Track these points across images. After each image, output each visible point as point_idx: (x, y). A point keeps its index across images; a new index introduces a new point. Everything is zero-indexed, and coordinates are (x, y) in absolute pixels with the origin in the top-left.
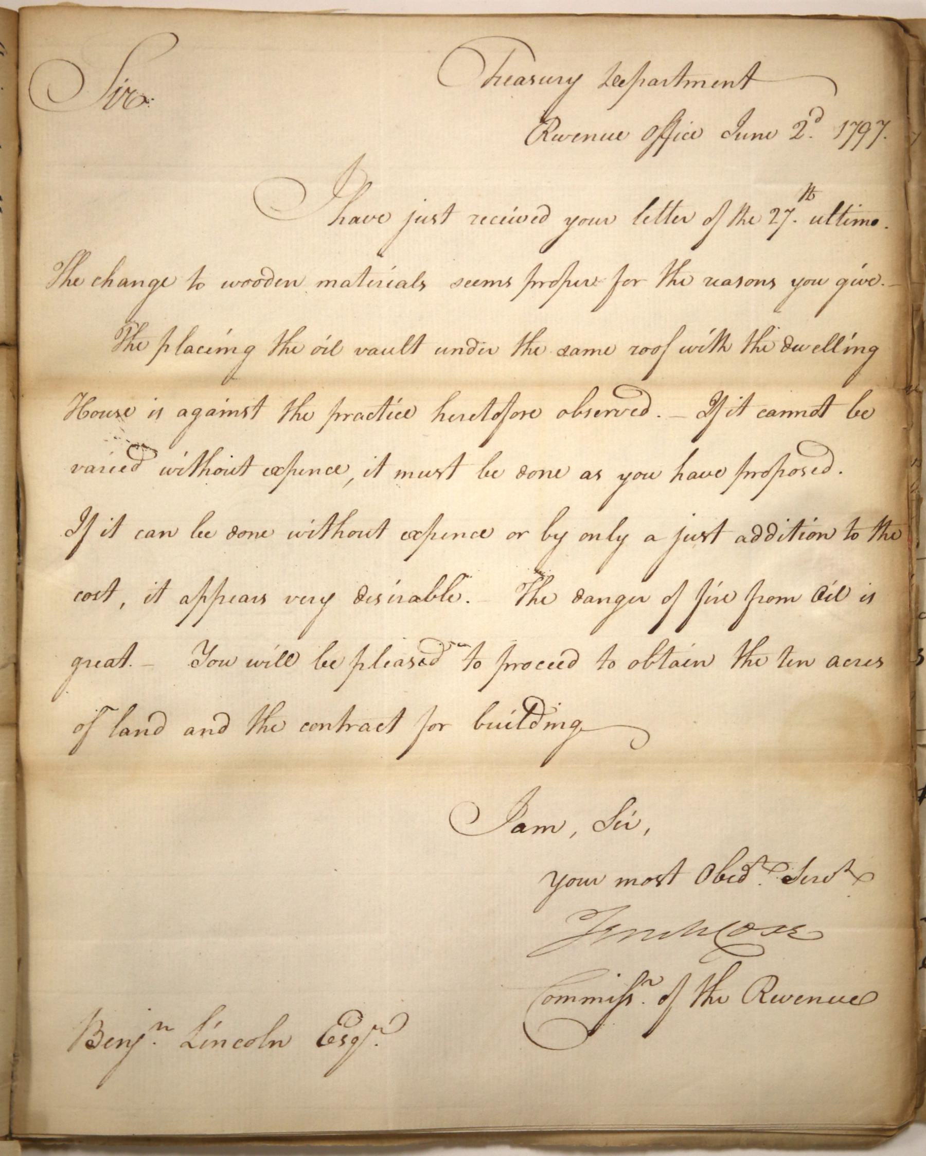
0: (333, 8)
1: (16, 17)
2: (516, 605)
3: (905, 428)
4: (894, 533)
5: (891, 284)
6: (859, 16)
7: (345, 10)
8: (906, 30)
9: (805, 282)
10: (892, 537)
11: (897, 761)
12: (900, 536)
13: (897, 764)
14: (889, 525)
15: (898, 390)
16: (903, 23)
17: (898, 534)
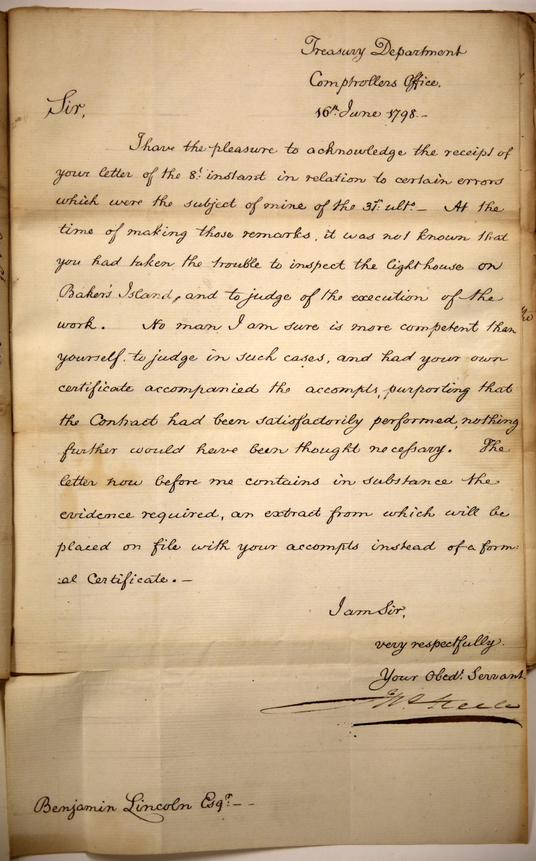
0: (194, 8)
1: (6, 17)
2: (358, 444)
3: (534, 255)
4: (528, 317)
5: (525, 170)
6: (504, 11)
7: (200, 9)
8: (532, 20)
9: (72, 358)
10: (527, 319)
11: (531, 451)
12: (532, 318)
13: (531, 453)
14: (525, 312)
15: (530, 233)
16: (530, 15)
17: (531, 317)
